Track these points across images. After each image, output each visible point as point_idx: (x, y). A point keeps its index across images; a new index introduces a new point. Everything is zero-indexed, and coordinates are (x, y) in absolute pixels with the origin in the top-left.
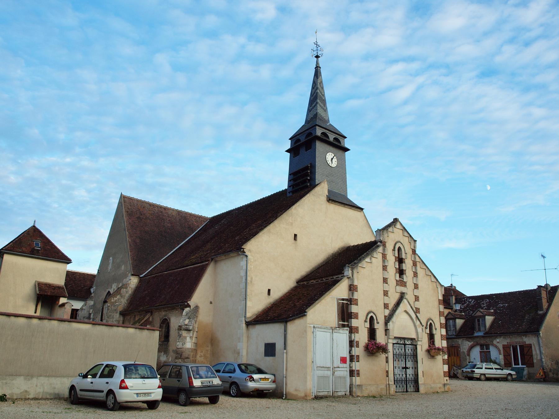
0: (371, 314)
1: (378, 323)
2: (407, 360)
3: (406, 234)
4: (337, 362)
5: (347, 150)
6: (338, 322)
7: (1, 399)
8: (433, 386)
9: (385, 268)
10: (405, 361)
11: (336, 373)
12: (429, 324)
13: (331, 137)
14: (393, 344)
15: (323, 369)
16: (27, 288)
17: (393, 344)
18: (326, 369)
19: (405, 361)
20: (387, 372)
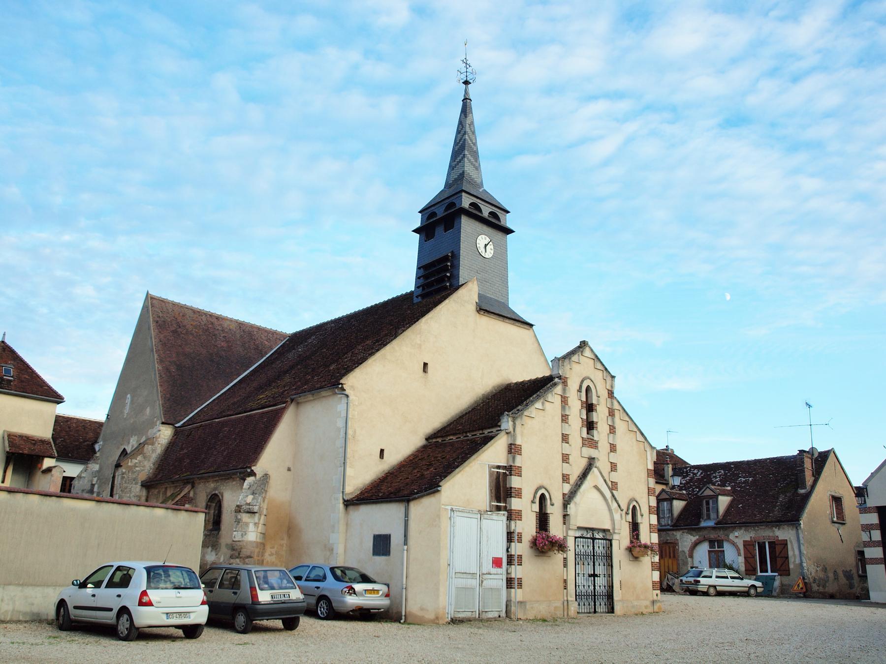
3: (599, 366)
4: (488, 566)
6: (490, 502)
8: (635, 603)
11: (485, 582)
15: (465, 576)
17: (576, 538)
18: (469, 576)
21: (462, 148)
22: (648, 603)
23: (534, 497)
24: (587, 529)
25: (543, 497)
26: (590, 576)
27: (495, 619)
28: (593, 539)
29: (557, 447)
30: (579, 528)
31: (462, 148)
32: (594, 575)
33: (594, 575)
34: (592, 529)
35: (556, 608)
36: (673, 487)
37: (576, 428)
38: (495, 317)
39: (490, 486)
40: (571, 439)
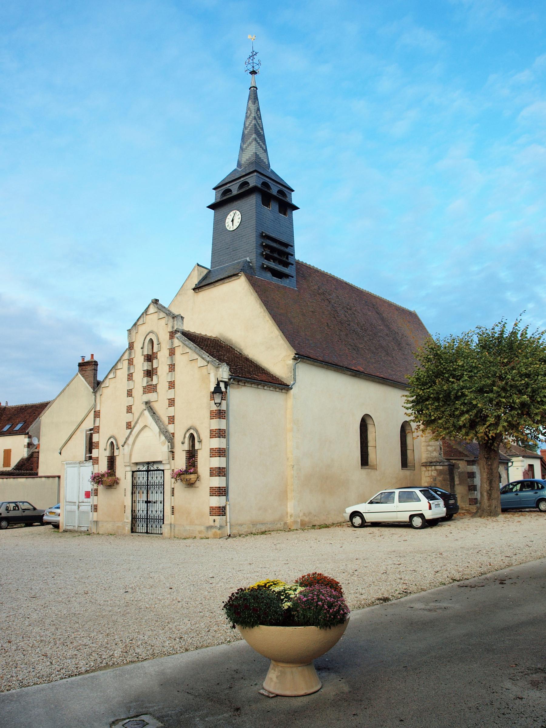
0: (112, 440)
1: (118, 449)
2: (150, 492)
3: (140, 322)
4: (82, 497)
5: (293, 191)
6: (86, 454)
7: (542, 671)
8: (188, 528)
9: (130, 377)
10: (147, 493)
11: (81, 508)
12: (188, 435)
13: (274, 190)
14: (133, 472)
15: (70, 504)
16: (89, 476)
17: (133, 472)
18: (73, 504)
19: (147, 493)
20: (173, 513)
21: (255, 132)
22: (202, 528)
23: (185, 437)
24: (143, 464)
25: (192, 436)
26: (150, 502)
27: (84, 532)
28: (148, 471)
29: (179, 394)
30: (137, 464)
31: (255, 132)
32: (147, 502)
33: (147, 502)
34: (148, 463)
35: (118, 527)
36: (458, 365)
37: (140, 381)
38: (207, 287)
39: (86, 444)
40: (134, 393)
